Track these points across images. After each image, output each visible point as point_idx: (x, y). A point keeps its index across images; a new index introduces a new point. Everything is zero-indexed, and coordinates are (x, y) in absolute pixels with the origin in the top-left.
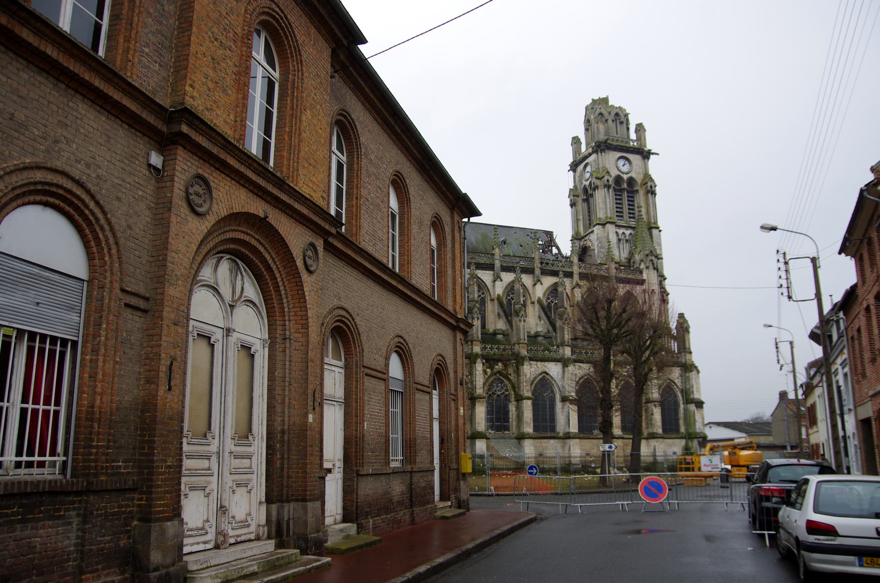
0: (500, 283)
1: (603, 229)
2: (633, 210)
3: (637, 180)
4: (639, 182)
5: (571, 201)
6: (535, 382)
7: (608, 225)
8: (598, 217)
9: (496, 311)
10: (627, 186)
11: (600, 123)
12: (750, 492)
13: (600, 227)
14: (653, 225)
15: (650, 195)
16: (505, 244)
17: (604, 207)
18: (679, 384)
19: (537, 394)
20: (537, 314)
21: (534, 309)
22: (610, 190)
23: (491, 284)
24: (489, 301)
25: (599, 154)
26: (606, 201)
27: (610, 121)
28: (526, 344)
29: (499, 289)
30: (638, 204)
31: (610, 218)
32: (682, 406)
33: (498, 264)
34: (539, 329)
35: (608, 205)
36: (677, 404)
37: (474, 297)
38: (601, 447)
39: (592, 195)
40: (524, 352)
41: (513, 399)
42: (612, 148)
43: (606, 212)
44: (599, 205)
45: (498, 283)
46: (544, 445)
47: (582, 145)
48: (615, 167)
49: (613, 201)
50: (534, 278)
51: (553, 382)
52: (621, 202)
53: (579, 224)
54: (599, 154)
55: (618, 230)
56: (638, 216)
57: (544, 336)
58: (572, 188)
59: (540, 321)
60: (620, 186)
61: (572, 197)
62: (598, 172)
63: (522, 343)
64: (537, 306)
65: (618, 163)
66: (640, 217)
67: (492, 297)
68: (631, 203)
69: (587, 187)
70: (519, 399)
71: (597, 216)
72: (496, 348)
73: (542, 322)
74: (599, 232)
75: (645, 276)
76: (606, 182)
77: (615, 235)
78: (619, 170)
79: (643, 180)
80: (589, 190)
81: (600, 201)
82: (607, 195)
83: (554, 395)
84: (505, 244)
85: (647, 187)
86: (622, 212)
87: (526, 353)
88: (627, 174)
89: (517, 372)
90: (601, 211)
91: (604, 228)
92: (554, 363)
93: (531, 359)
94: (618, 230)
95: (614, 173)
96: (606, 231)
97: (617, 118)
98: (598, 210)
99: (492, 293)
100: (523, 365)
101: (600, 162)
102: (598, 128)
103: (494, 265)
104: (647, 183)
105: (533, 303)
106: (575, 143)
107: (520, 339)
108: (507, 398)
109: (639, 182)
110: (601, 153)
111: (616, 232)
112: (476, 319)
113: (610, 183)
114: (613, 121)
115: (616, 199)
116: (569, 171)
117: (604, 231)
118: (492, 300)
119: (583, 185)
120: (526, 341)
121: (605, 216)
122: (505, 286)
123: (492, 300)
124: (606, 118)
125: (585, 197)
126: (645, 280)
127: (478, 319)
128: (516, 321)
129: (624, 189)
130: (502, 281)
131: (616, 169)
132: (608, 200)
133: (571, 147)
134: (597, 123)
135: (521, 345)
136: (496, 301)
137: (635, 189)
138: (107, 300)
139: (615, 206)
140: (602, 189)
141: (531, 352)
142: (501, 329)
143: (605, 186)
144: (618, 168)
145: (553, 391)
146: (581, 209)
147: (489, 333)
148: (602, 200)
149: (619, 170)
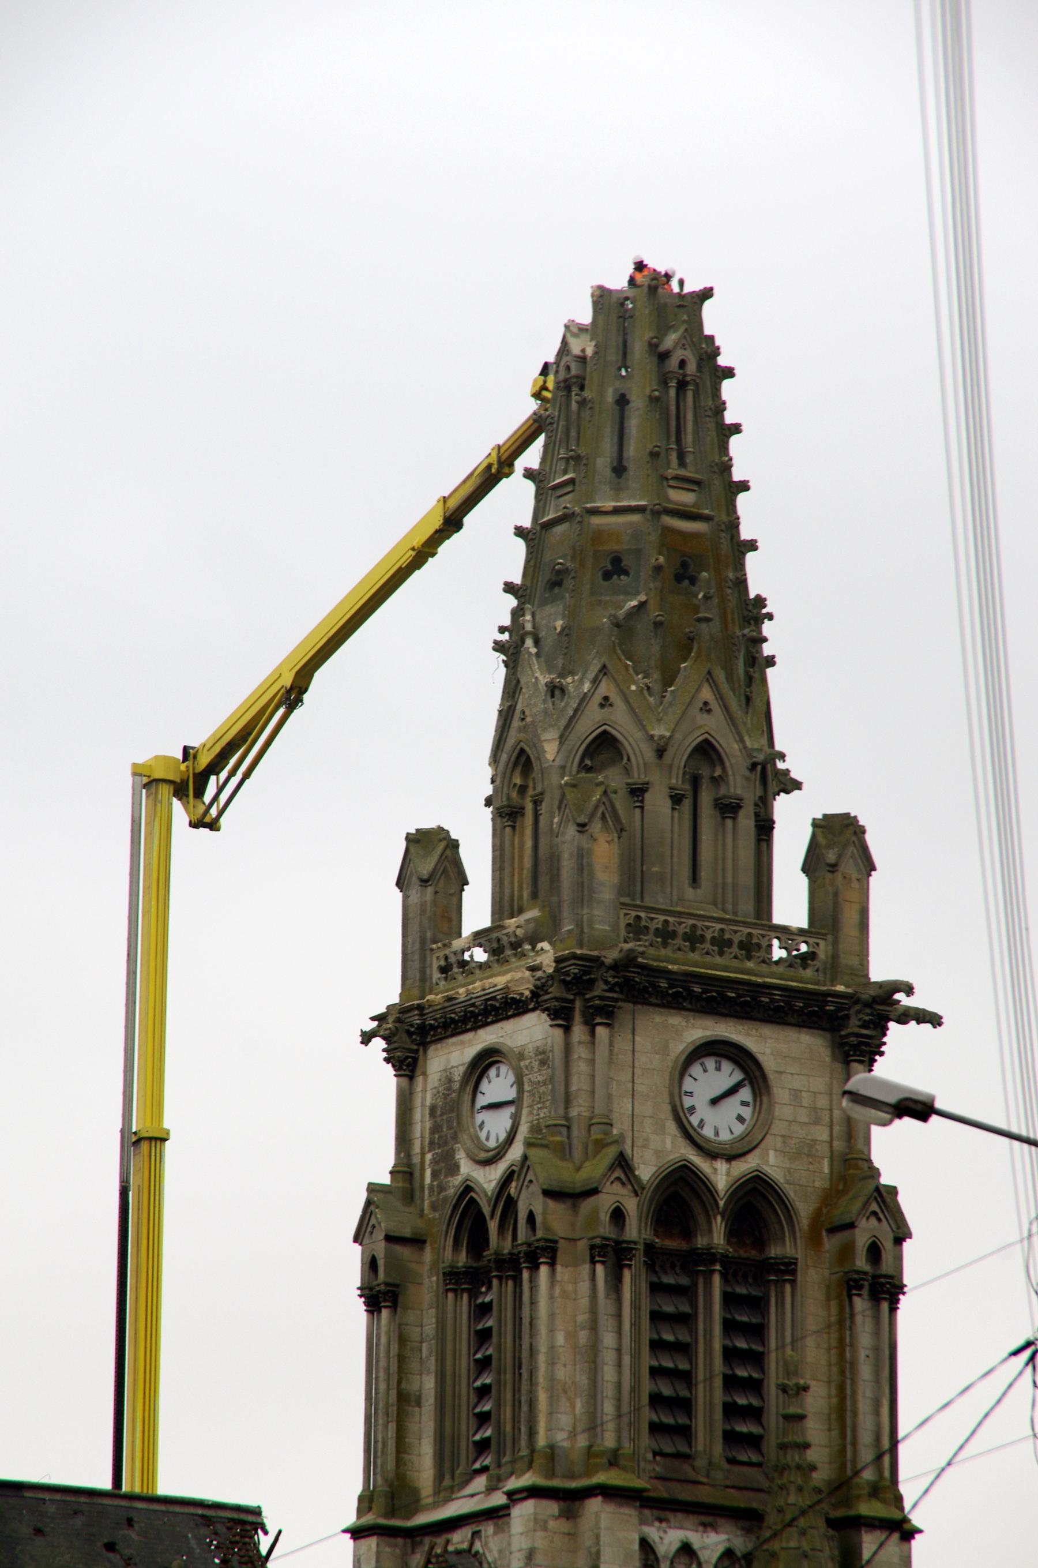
1: (563, 1525)
2: (754, 1442)
3: (791, 1192)
4: (804, 1209)
5: (371, 1265)
7: (595, 1505)
8: (541, 1441)
10: (732, 1234)
11: (596, 827)
13: (552, 1507)
14: (867, 1509)
15: (860, 1304)
17: (583, 1381)
22: (627, 1275)
25: (579, 1031)
26: (594, 1347)
27: (658, 801)
30: (791, 1369)
31: (614, 1460)
35: (609, 1374)
42: (662, 994)
43: (593, 1426)
44: (552, 1363)
47: (469, 896)
48: (667, 1108)
49: (636, 1356)
52: (684, 1337)
53: (412, 1427)
54: (579, 1031)
55: (653, 1533)
56: (783, 1447)
58: (386, 1179)
60: (688, 1234)
61: (380, 1248)
62: (563, 1151)
65: (688, 1084)
66: (793, 1457)
68: (742, 1344)
69: (486, 1210)
71: (532, 1433)
74: (540, 1541)
76: (605, 1229)
78: (689, 1135)
79: (830, 1197)
80: (493, 1226)
81: (560, 1339)
82: (605, 1306)
85: (846, 1252)
86: (683, 1349)
88: (730, 1158)
90: (564, 1404)
91: (570, 1515)
94: (653, 1533)
97: (705, 771)
98: (542, 1397)
101: (579, 1083)
102: (583, 861)
104: (851, 1226)
106: (424, 882)
109: (804, 1209)
110: (592, 1029)
114: (677, 799)
115: (656, 1372)
116: (366, 1038)
117: (572, 1536)
119: (457, 1181)
121: (582, 1442)
124: (638, 777)
125: (462, 1259)
129: (709, 1256)
131: (672, 1127)
132: (608, 1339)
133: (398, 895)
134: (582, 827)
137: (774, 1251)
139: (648, 1415)
140: (576, 1264)
144: (680, 1118)
146: (430, 1328)
148: (571, 1336)
149: (689, 1135)
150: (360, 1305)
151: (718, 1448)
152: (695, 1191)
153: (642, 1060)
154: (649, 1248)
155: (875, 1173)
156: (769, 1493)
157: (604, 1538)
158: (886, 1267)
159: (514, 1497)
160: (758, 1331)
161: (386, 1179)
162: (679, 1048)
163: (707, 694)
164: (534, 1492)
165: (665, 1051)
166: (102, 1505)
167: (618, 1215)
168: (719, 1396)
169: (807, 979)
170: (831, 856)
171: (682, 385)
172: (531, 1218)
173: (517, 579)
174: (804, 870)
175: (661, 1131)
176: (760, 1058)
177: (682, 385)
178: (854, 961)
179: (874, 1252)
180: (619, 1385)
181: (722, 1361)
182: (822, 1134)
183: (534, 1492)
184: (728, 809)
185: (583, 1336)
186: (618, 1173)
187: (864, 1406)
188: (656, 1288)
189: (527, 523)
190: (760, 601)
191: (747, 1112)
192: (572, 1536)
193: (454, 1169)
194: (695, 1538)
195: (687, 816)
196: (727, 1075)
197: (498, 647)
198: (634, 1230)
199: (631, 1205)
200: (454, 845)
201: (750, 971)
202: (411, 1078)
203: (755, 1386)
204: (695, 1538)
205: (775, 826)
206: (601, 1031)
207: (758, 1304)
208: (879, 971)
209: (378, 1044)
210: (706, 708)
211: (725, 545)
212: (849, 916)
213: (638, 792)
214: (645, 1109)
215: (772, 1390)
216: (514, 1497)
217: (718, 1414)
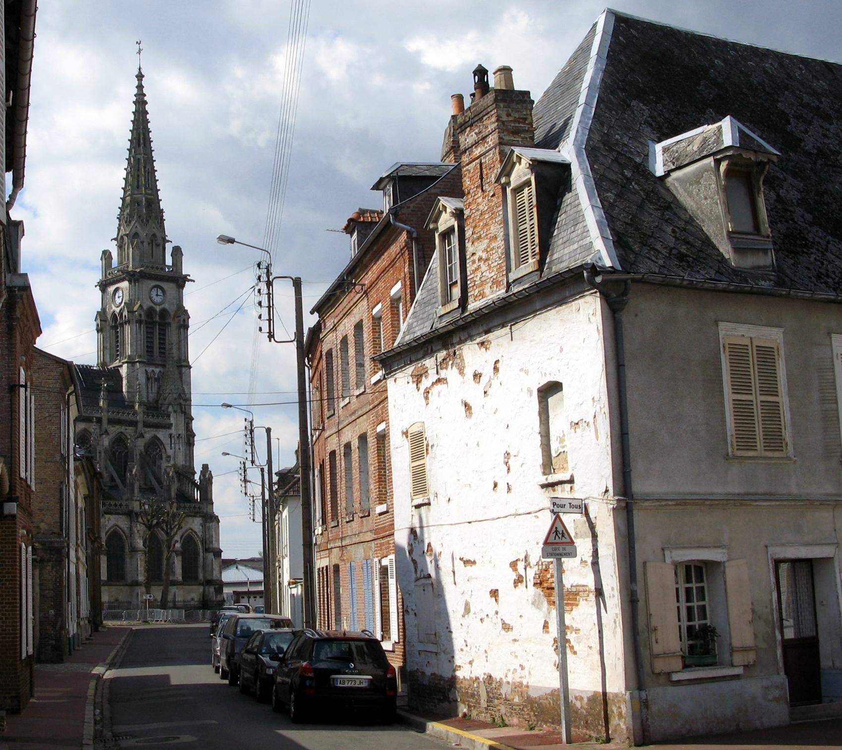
3: (170, 311)
4: (172, 314)
12: (152, 312)
13: (130, 365)
14: (184, 364)
15: (182, 330)
18: (200, 534)
25: (133, 284)
27: (145, 244)
32: (201, 554)
36: (197, 554)
43: (137, 351)
48: (148, 297)
55: (147, 369)
56: (169, 354)
58: (100, 310)
75: (172, 420)
80: (119, 318)
85: (180, 320)
94: (147, 369)
97: (154, 239)
109: (172, 314)
114: (149, 244)
116: (96, 286)
119: (112, 310)
126: (172, 424)
144: (151, 298)
150: (96, 331)
151: (158, 353)
153: (144, 288)
154: (146, 321)
155: (184, 307)
156: (502, 716)
158: (186, 323)
159: (123, 363)
160: (164, 335)
161: (100, 310)
162: (150, 286)
163: (154, 225)
164: (126, 362)
166: (807, 544)
167: (140, 315)
168: (158, 346)
169: (172, 274)
170: (176, 253)
171: (148, 173)
172: (125, 316)
173: (121, 206)
174: (171, 255)
176: (164, 288)
177: (148, 173)
178: (180, 271)
179: (184, 321)
181: (444, 723)
182: (175, 301)
183: (126, 362)
184: (158, 245)
185: (135, 336)
187: (183, 347)
188: (147, 327)
189: (122, 197)
190: (163, 209)
191: (162, 297)
193: (112, 308)
194: (154, 369)
195: (151, 248)
196: (160, 292)
197: (118, 218)
198: (143, 318)
199: (143, 314)
200: (110, 253)
201: (162, 273)
203: (164, 344)
204: (154, 369)
205: (132, 117)
206: (137, 284)
207: (164, 330)
208: (184, 273)
209: (98, 287)
210: (154, 228)
211: (157, 201)
212: (179, 264)
213: (142, 243)
215: (167, 344)
216: (123, 363)
217: (158, 349)
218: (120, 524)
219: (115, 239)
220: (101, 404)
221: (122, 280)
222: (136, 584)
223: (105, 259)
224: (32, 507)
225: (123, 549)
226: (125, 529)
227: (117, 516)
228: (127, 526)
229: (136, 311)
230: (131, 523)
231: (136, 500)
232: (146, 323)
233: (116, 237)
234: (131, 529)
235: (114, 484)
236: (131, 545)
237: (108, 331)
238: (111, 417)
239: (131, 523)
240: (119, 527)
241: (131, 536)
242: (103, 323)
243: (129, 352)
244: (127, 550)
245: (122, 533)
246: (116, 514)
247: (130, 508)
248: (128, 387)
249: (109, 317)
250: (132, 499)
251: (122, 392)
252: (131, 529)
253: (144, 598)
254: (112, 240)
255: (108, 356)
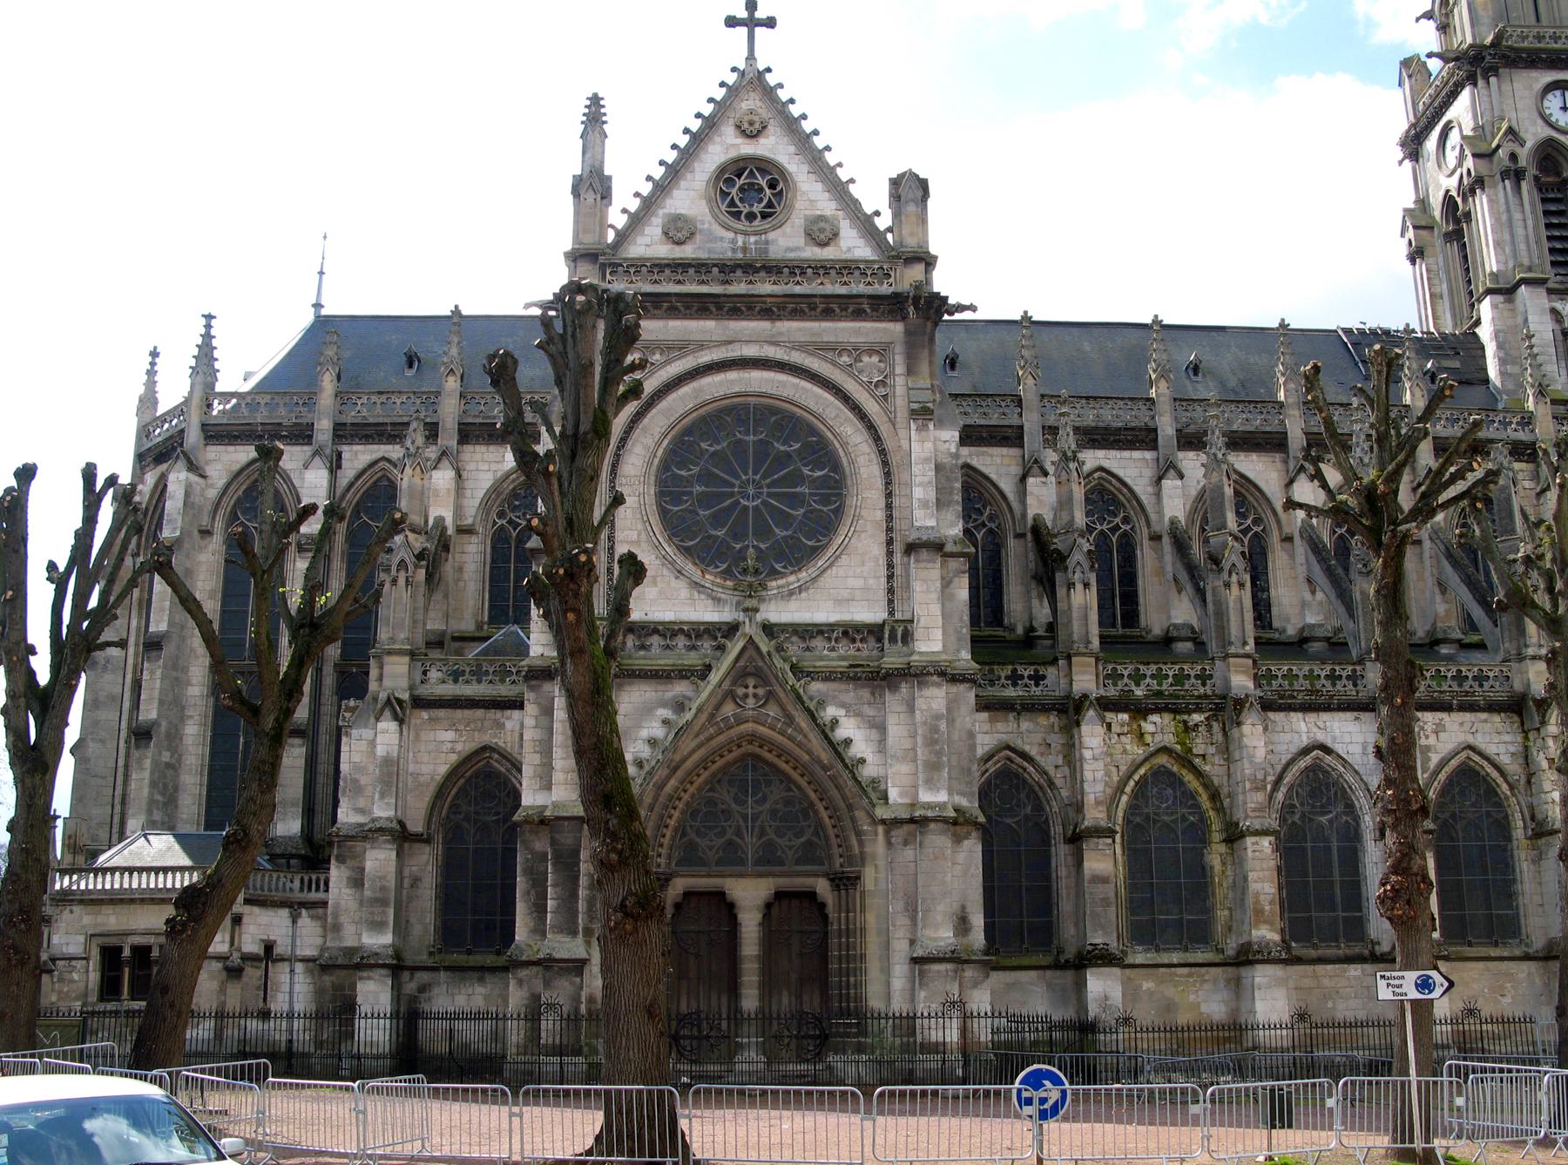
0: (1179, 483)
1: (1508, 306)
6: (1287, 779)
9: (1169, 568)
12: (1555, 154)
13: (1500, 298)
16: (1196, 374)
19: (1296, 817)
20: (1302, 571)
21: (1292, 556)
22: (1524, 185)
23: (1150, 489)
24: (1146, 542)
25: (1481, 83)
26: (1510, 220)
28: (1247, 656)
29: (1175, 503)
31: (1530, 269)
33: (1167, 428)
34: (1311, 619)
35: (1520, 231)
37: (1072, 521)
38: (1382, 984)
39: (1468, 215)
40: (1241, 682)
41: (1216, 837)
45: (1169, 484)
46: (1326, 982)
48: (1535, 115)
50: (1285, 462)
51: (1349, 777)
54: (1481, 83)
55: (1558, 305)
57: (1327, 639)
59: (1313, 592)
60: (1558, 174)
61: (1411, 233)
63: (1237, 656)
64: (1300, 547)
65: (1546, 104)
67: (1156, 528)
70: (1234, 836)
72: (1153, 676)
73: (1320, 595)
76: (1507, 163)
77: (1548, 318)
80: (1459, 200)
83: (1357, 819)
84: (1196, 374)
87: (1251, 685)
89: (1227, 750)
91: (1510, 301)
92: (1349, 715)
93: (1267, 706)
94: (1558, 305)
95: (1534, 133)
96: (1521, 308)
99: (1153, 517)
100: (1239, 724)
103: (1155, 430)
105: (1288, 539)
107: (1230, 643)
108: (1199, 833)
111: (1554, 311)
112: (1079, 587)
113: (1522, 162)
118: (1156, 538)
120: (1250, 648)
122: (1194, 492)
123: (1156, 538)
127: (1086, 585)
128: (1214, 589)
130: (1181, 477)
131: (1540, 122)
132: (1517, 216)
135: (1231, 660)
136: (1166, 540)
138: (807, 757)
141: (1270, 684)
142: (1185, 625)
143: (1505, 175)
145: (1350, 807)
147: (1150, 638)
152: (1561, 153)
157: (1528, 304)
165: (1531, 88)
167: (1513, 157)
172: (1469, 171)
175: (1535, 123)
180: (1527, 236)
186: (1510, 137)
192: (1513, 310)
202: (1417, 161)
214: (1523, 115)
218: (1480, 741)
219: (1428, 15)
220: (1407, 399)
221: (1453, 95)
222: (1246, 957)
223: (1410, 76)
224: (285, 422)
225: (1503, 827)
226: (1505, 760)
227: (1467, 717)
228: (1512, 749)
229: (1498, 147)
230: (1526, 738)
231: (1534, 658)
232: (1539, 185)
233: (1429, 7)
234: (1526, 757)
235: (1475, 638)
236: (1533, 818)
237: (1443, 255)
238: (1443, 434)
239: (1526, 738)
240: (1480, 754)
241: (1529, 782)
242: (1424, 233)
243: (1491, 261)
244: (1519, 832)
245: (1495, 774)
246: (1463, 708)
247: (1518, 686)
248: (1503, 362)
249: (1437, 214)
250: (1521, 658)
251: (1486, 381)
252: (1526, 757)
253: (1385, 993)
254: (1418, 20)
255: (1448, 315)
